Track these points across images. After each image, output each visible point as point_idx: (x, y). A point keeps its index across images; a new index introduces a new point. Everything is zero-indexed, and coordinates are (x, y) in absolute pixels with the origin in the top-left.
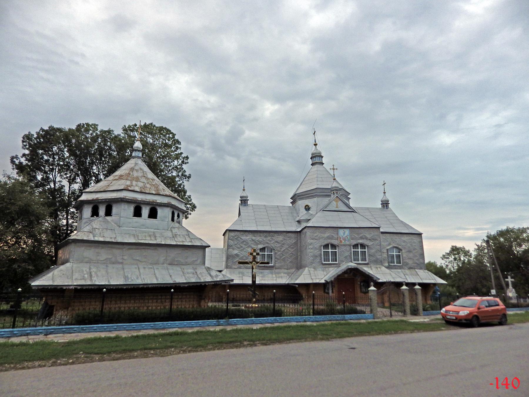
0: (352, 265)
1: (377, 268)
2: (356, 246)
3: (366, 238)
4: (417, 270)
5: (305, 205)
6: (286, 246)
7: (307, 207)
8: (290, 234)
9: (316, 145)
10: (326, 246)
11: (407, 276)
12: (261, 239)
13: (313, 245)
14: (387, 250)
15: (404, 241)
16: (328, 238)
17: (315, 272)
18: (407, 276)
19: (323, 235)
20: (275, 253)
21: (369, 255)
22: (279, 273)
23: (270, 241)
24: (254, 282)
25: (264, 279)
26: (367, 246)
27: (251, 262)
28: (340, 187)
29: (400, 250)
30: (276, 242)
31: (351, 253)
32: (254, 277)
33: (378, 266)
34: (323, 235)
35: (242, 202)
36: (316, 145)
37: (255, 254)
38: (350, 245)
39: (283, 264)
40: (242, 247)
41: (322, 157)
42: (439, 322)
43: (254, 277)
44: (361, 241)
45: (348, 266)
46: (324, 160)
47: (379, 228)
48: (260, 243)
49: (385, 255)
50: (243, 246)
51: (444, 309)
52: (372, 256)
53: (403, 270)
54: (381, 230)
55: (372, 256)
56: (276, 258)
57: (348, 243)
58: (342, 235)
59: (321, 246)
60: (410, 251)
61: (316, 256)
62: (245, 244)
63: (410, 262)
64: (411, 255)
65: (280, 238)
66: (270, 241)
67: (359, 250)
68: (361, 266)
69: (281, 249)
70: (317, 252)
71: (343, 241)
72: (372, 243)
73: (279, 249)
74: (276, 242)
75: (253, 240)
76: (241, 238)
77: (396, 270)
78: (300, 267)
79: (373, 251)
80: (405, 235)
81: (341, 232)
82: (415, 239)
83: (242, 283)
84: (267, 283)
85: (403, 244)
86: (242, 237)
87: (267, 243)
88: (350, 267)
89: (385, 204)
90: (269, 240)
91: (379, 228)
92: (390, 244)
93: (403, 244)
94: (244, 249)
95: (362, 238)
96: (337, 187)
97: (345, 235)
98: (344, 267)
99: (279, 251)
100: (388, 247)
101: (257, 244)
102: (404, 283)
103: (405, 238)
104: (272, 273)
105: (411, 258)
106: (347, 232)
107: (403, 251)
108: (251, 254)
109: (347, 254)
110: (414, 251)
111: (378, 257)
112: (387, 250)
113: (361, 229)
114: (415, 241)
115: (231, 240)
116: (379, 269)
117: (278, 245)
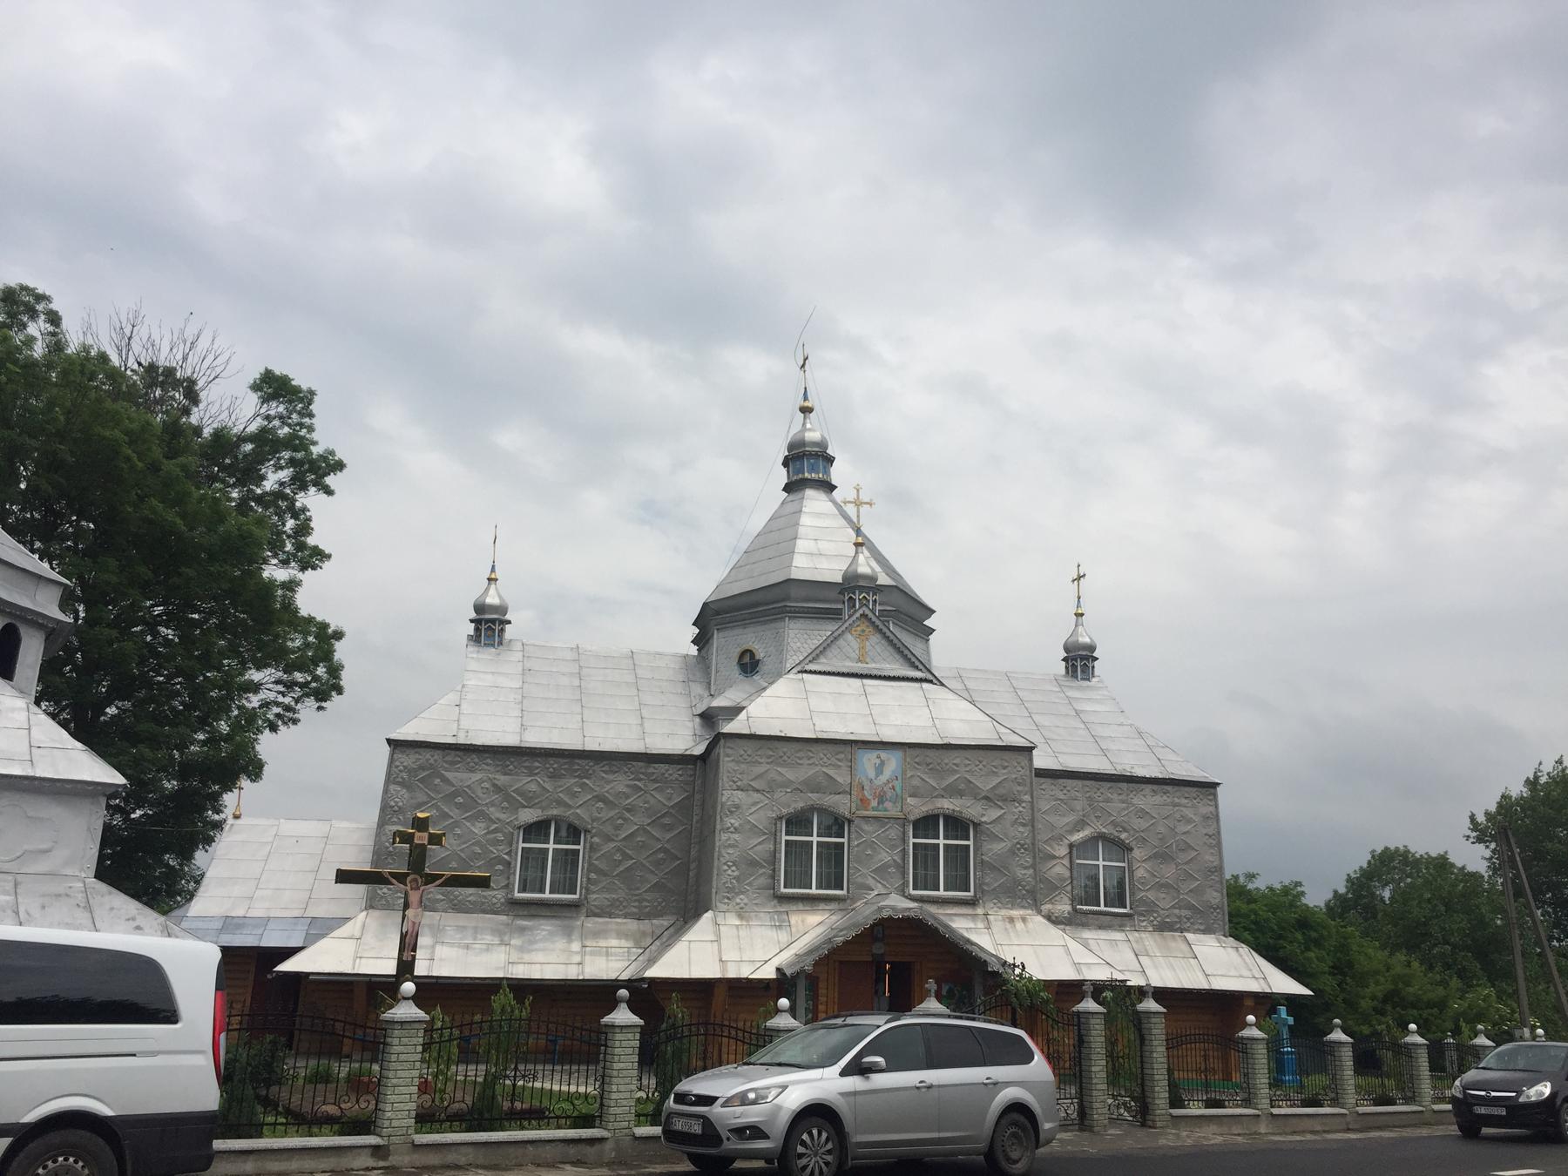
0: (898, 904)
1: (1011, 920)
2: (926, 825)
3: (975, 794)
4: (1190, 936)
5: (746, 647)
6: (640, 820)
7: (747, 659)
8: (663, 767)
9: (806, 410)
10: (797, 822)
11: (1144, 960)
12: (533, 787)
13: (746, 814)
14: (1071, 846)
15: (1142, 814)
16: (813, 786)
17: (743, 933)
18: (1144, 960)
19: (790, 774)
20: (593, 848)
21: (982, 864)
22: (597, 934)
23: (574, 795)
24: (405, 967)
25: (527, 957)
26: (976, 825)
27: (401, 878)
28: (883, 580)
29: (1119, 847)
30: (599, 798)
31: (904, 852)
32: (408, 945)
33: (1015, 913)
34: (790, 774)
35: (477, 630)
36: (806, 410)
37: (421, 838)
38: (903, 821)
39: (621, 895)
40: (446, 816)
41: (830, 460)
42: (1439, 1131)
43: (408, 945)
44: (947, 805)
45: (880, 909)
46: (837, 473)
47: (1029, 750)
48: (530, 801)
49: (1060, 870)
50: (455, 813)
51: (1457, 1083)
52: (993, 868)
53: (1134, 936)
54: (1041, 760)
55: (993, 868)
56: (591, 868)
57: (893, 810)
58: (872, 773)
59: (780, 818)
60: (1162, 856)
61: (753, 864)
62: (459, 806)
63: (1164, 901)
64: (1169, 872)
65: (618, 783)
66: (574, 795)
67: (941, 842)
68: (933, 909)
69: (618, 828)
70: (758, 847)
71: (874, 803)
72: (994, 814)
73: (608, 829)
74: (599, 798)
75: (498, 789)
76: (446, 780)
77: (1103, 935)
78: (685, 902)
79: (995, 849)
80: (1148, 788)
81: (868, 760)
82: (1193, 808)
83: (572, 973)
84: (537, 976)
85: (1138, 824)
86: (449, 775)
87: (560, 803)
88: (885, 914)
89: (1079, 660)
90: (569, 791)
91: (1029, 750)
92: (1080, 824)
93: (1138, 824)
94: (456, 824)
95: (953, 791)
96: (873, 578)
97: (884, 778)
98: (865, 911)
99: (609, 839)
100: (1077, 837)
101: (515, 806)
102: (1088, 988)
103: (1146, 800)
104: (568, 933)
105: (1167, 886)
106: (893, 762)
107: (1137, 853)
108: (406, 838)
109: (885, 856)
110: (1183, 857)
111: (1020, 873)
112: (1071, 846)
113: (955, 753)
114: (1189, 813)
115: (402, 784)
116: (1019, 925)
117: (607, 814)
